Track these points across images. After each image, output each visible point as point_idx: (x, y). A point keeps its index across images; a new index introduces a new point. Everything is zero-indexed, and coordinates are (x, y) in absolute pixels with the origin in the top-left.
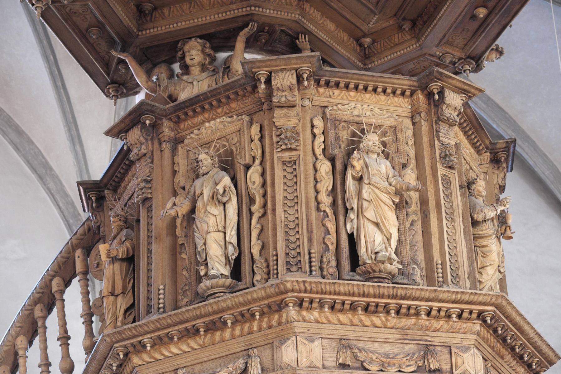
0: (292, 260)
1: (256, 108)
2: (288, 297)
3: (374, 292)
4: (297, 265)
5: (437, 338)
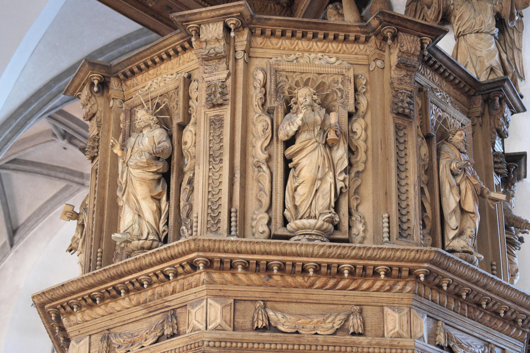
3: (94, 281)
5: (174, 301)
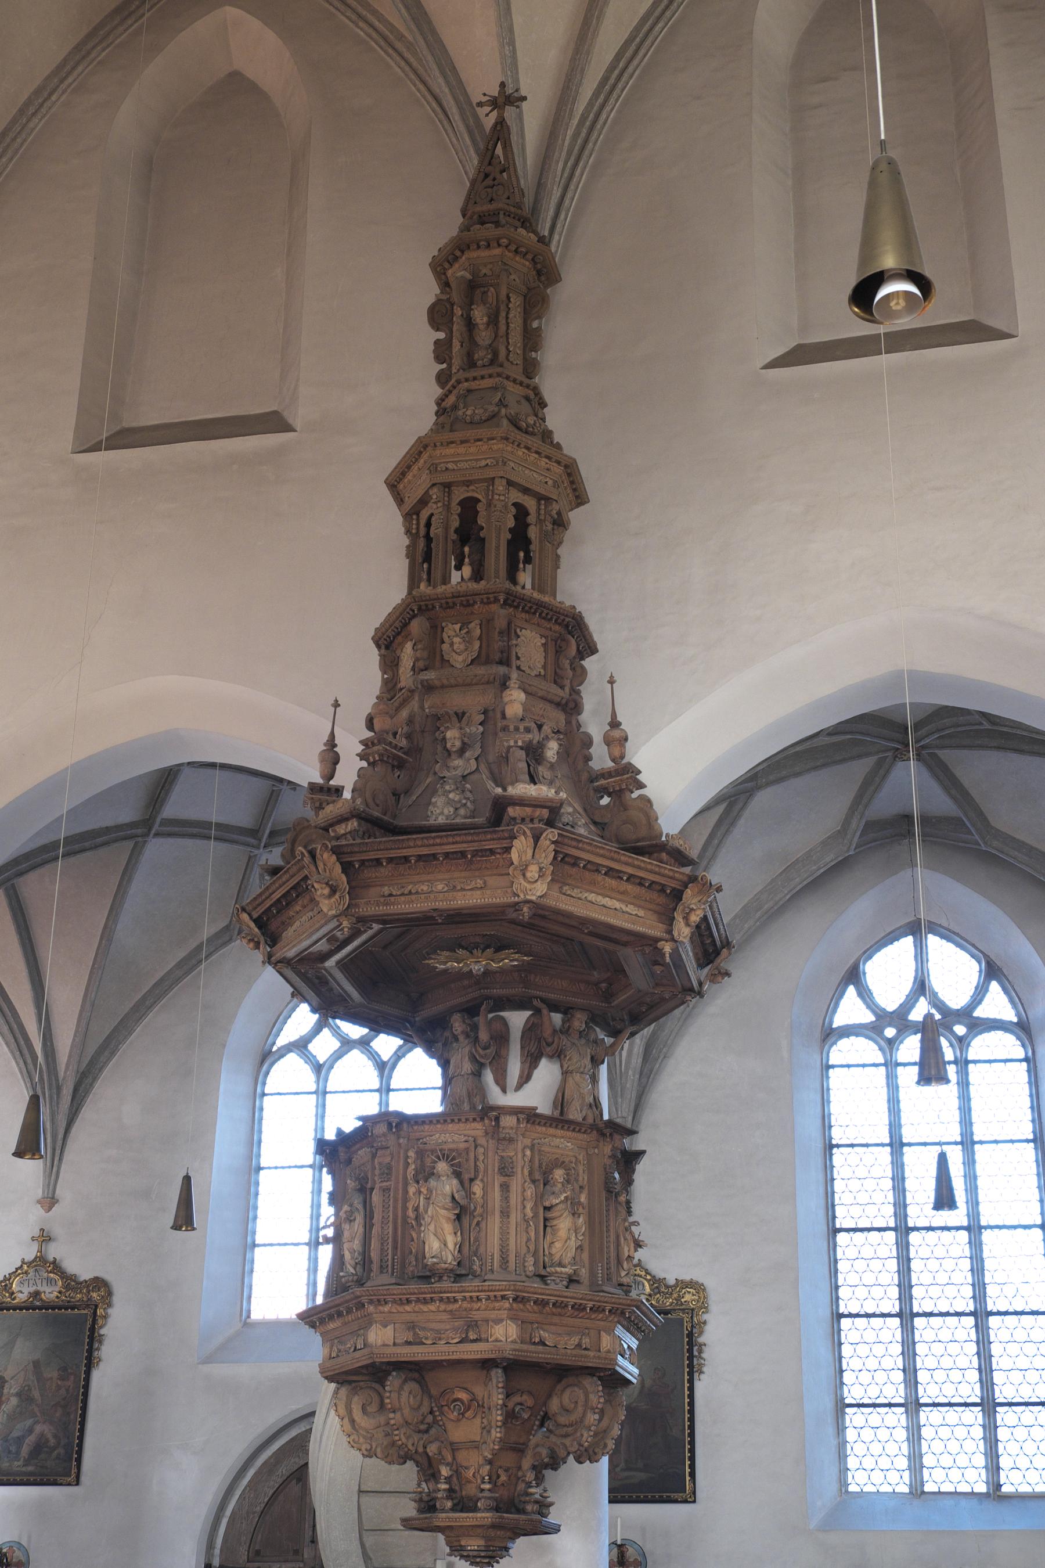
5: (477, 1315)
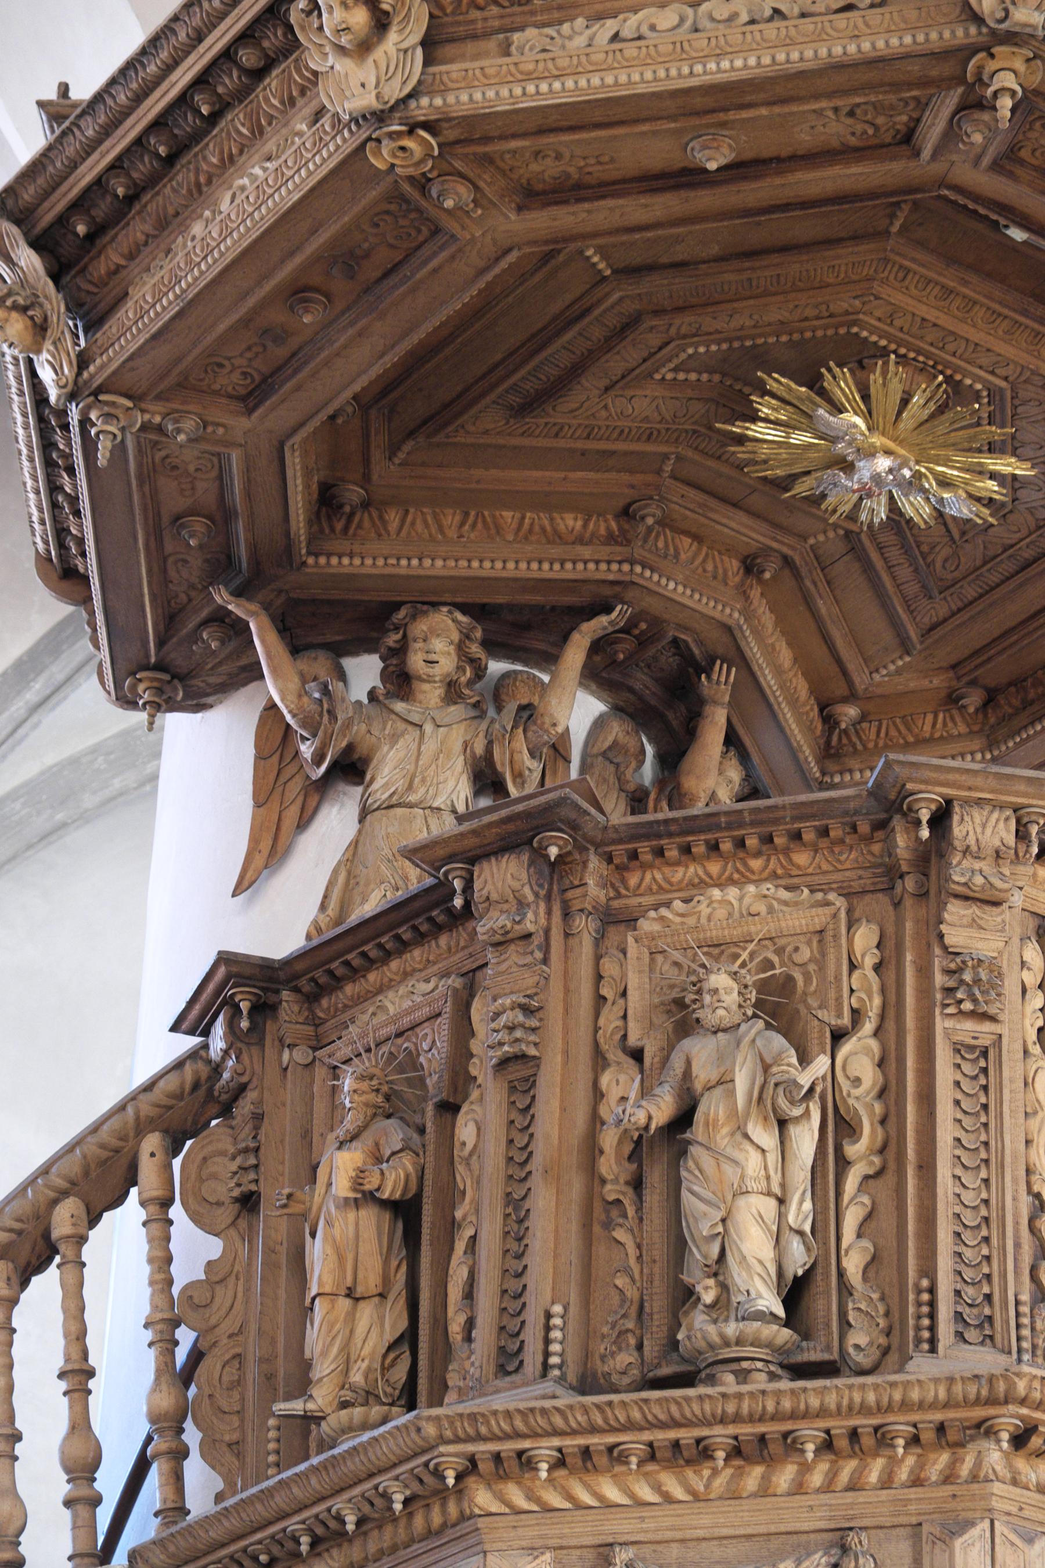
0: (967, 1310)
1: (869, 881)
2: (1004, 1416)
4: (980, 1326)
